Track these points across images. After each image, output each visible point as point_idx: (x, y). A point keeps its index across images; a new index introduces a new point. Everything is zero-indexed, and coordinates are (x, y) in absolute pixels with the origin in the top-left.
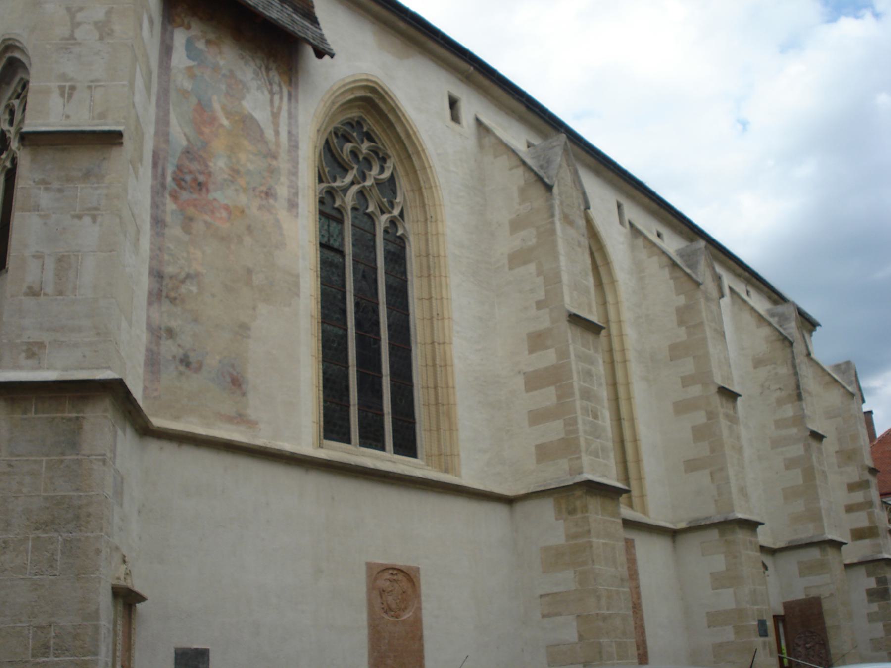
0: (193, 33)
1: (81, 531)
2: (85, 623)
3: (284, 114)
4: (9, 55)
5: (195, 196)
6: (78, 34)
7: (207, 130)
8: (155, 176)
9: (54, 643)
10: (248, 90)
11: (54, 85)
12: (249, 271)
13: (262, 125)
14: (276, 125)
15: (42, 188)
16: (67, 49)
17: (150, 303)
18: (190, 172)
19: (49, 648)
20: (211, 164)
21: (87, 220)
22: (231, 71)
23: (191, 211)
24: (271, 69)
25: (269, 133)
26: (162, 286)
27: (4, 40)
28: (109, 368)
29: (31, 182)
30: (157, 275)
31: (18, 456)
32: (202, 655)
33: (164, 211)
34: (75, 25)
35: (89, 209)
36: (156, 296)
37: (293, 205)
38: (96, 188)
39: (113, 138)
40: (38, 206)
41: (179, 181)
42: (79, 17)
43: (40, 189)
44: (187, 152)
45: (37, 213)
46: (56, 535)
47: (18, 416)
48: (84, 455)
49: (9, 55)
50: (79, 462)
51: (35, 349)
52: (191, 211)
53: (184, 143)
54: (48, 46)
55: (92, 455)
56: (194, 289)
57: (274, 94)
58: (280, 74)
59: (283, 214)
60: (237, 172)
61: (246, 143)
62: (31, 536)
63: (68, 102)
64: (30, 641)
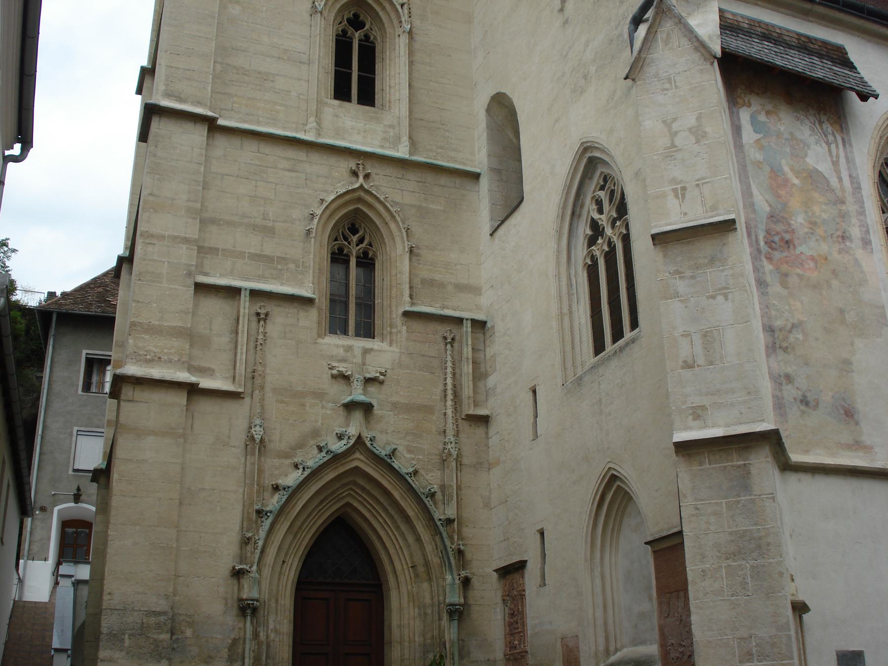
0: (755, 109)
1: (764, 558)
2: (780, 634)
3: (842, 160)
4: (588, 155)
5: (785, 254)
6: (678, 141)
7: (783, 193)
8: (751, 245)
9: (756, 651)
10: (809, 147)
11: (668, 189)
12: (842, 311)
13: (826, 175)
14: (838, 172)
16: (671, 156)
17: (768, 356)
18: (778, 233)
19: (752, 655)
20: (792, 222)
21: (720, 298)
22: (791, 133)
23: (785, 268)
24: (824, 122)
25: (834, 182)
26: (775, 339)
28: (763, 421)
29: (667, 274)
30: (769, 330)
31: (702, 500)
32: (858, 656)
33: (764, 273)
34: (673, 135)
35: (720, 290)
36: (772, 348)
37: (866, 243)
38: (722, 271)
39: (728, 226)
40: (678, 293)
41: (769, 243)
42: (675, 126)
43: (676, 278)
44: (771, 216)
46: (744, 562)
47: (696, 468)
48: (756, 495)
49: (588, 155)
50: (753, 501)
51: (699, 412)
52: (785, 268)
53: (768, 209)
54: (655, 157)
55: (762, 495)
56: (800, 337)
57: (831, 144)
58: (831, 124)
59: (860, 253)
60: (814, 223)
61: (816, 195)
62: (724, 565)
64: (736, 649)
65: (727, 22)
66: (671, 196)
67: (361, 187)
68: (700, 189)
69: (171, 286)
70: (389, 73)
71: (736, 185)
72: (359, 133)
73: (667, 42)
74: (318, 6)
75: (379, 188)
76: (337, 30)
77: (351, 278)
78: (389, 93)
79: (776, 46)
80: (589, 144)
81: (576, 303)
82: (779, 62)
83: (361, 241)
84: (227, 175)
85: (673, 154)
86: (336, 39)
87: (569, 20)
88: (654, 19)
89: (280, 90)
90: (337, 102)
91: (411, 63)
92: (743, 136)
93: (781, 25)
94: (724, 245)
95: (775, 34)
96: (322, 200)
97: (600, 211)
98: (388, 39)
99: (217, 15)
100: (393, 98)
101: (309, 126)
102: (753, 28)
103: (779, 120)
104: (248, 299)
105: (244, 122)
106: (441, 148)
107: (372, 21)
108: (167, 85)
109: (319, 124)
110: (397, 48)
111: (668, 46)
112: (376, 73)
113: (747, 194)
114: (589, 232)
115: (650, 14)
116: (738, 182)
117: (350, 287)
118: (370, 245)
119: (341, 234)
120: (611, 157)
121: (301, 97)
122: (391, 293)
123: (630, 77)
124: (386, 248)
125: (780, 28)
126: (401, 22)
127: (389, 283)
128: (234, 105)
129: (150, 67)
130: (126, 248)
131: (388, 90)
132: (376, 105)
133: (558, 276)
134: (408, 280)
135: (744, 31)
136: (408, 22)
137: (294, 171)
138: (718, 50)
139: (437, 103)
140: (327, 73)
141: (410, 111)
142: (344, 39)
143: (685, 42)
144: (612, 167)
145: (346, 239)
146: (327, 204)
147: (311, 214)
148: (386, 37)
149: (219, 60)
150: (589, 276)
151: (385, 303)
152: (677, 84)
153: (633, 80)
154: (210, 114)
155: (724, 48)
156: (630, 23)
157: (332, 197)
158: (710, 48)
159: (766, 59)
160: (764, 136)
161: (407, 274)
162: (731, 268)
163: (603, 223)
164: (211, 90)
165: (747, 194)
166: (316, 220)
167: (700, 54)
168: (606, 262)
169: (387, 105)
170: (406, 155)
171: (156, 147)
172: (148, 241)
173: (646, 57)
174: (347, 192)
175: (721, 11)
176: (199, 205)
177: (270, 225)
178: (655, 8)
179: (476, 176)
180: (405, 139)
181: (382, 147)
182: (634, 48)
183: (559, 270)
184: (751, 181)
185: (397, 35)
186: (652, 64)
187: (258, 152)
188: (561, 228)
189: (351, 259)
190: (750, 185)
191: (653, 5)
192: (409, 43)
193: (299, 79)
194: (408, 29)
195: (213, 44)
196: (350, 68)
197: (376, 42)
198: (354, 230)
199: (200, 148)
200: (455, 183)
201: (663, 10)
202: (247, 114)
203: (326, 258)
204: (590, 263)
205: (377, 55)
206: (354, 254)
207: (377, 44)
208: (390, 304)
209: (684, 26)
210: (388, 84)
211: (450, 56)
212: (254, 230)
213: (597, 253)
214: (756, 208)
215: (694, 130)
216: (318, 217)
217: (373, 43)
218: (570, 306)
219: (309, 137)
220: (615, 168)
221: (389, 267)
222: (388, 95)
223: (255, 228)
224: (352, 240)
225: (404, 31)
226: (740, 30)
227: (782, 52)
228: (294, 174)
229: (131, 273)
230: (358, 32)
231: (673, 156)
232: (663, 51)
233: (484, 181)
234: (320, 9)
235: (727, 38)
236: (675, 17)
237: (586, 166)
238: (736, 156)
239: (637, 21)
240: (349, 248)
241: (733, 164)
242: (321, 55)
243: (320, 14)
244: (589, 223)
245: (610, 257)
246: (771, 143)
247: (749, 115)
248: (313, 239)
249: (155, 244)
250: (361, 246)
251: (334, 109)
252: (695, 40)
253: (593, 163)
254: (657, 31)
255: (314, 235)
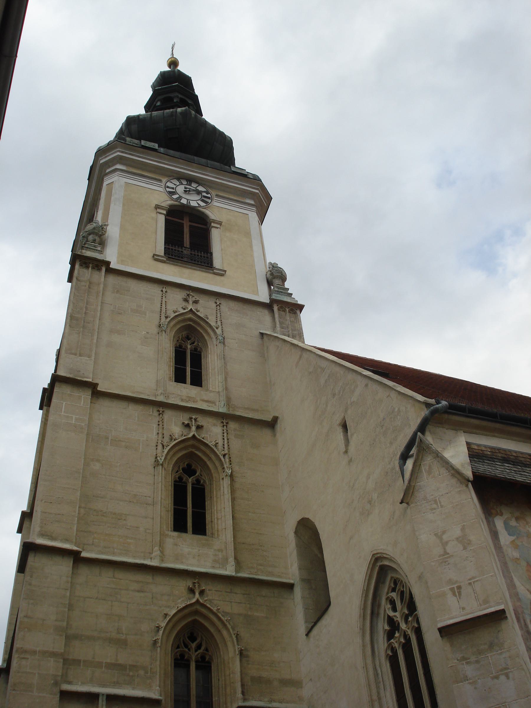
0: (506, 517)
4: (379, 564)
6: (449, 549)
8: (521, 628)
11: (446, 589)
15: (465, 663)
21: (503, 678)
27: (373, 555)
29: (456, 661)
34: (445, 544)
35: (501, 670)
38: (501, 653)
42: (445, 537)
43: (463, 664)
45: (467, 682)
49: (379, 564)
54: (433, 564)
63: (460, 598)
65: (474, 452)
66: (450, 595)
67: (198, 601)
68: (472, 587)
69: (41, 694)
70: (217, 509)
71: (502, 581)
72: (194, 558)
73: (429, 472)
74: (159, 460)
75: (213, 601)
76: (175, 477)
77: (191, 680)
78: (217, 524)
79: (514, 466)
80: (379, 555)
81: (383, 690)
82: (519, 478)
83: (199, 647)
84: (88, 598)
85: (446, 560)
86: (174, 484)
87: (353, 459)
88: (418, 455)
89: (131, 526)
90: (176, 534)
91: (233, 499)
92: (500, 539)
93: (516, 450)
94: (499, 632)
95: (512, 457)
96: (166, 615)
97: (394, 609)
98: (214, 482)
99: (82, 471)
100: (220, 528)
101: (154, 554)
102: (495, 454)
103: (527, 524)
104: (104, 703)
105: (102, 553)
106: (261, 565)
107: (202, 469)
108: (41, 527)
109: (162, 552)
110: (222, 488)
111: (431, 476)
112: (206, 508)
113: (511, 586)
114: (387, 627)
115: (414, 451)
116: (503, 577)
117: (191, 688)
118: (207, 650)
119: (182, 642)
120: (399, 565)
121: (148, 531)
122: (225, 691)
123: (404, 501)
124: (220, 652)
125: (516, 452)
126: (224, 468)
127: (223, 683)
128: (94, 540)
129: (29, 511)
130: (4, 661)
131: (216, 521)
132: (207, 534)
133: (366, 667)
134: (239, 679)
135: (488, 458)
136: (229, 468)
137: (143, 592)
138: (469, 474)
139: (255, 529)
140: (168, 511)
141: (235, 537)
142: (180, 484)
143: (443, 471)
144: (399, 572)
145: (186, 646)
146: (170, 617)
147: (157, 627)
148: (213, 481)
149: (83, 505)
150: (391, 666)
151: (221, 700)
152: (442, 504)
153: (408, 503)
154: (75, 548)
155: (475, 472)
156: (400, 459)
157: (174, 611)
158: (464, 474)
159: (509, 477)
160: (517, 537)
161: (239, 674)
162: (508, 651)
163: (397, 619)
164: (77, 528)
165: (511, 586)
166: (161, 632)
167: (456, 479)
168: (404, 652)
169: (216, 533)
170: (233, 573)
171: (31, 577)
172: (22, 656)
173: (415, 485)
174: (184, 608)
175: (468, 444)
176: (65, 624)
177: (123, 638)
178: (417, 447)
179: (290, 587)
180: (231, 560)
181: (213, 567)
182: (405, 478)
183: (365, 662)
184: (513, 574)
185: (221, 478)
186: (420, 490)
187: (114, 577)
188: (364, 625)
189: (191, 663)
190: (512, 579)
191: (415, 444)
192: (231, 484)
193: (146, 518)
194: (230, 474)
195: (79, 494)
196: (186, 506)
197: (205, 485)
198: (193, 638)
199: (67, 577)
200: (274, 593)
201: (424, 448)
202: (105, 547)
203: (170, 663)
204: (391, 654)
205: (206, 494)
206: (194, 658)
207: (206, 486)
208: (226, 701)
209: (441, 459)
210: (216, 516)
211: (263, 491)
212: (110, 643)
213: (396, 645)
214: (520, 597)
215: (461, 539)
216: (163, 629)
217: (203, 485)
218: (379, 693)
219: (154, 563)
220: (402, 573)
221: (223, 668)
222: (216, 526)
223: (111, 641)
224: (191, 647)
225: (227, 475)
226: (485, 457)
227: (520, 470)
228: (142, 594)
229: (7, 683)
230: (191, 478)
231: (447, 561)
232: (427, 480)
233: (298, 591)
234: (161, 463)
235: (475, 465)
236: (433, 453)
237: (378, 573)
238: (498, 556)
239: (404, 457)
240: (189, 654)
241: (496, 563)
242: (163, 497)
243: (161, 466)
244: (386, 621)
245: (407, 647)
246: (524, 543)
247: (503, 522)
248: (159, 649)
249: (28, 659)
250: (199, 651)
251: (174, 539)
252: (451, 469)
253: (384, 571)
254: (420, 465)
255: (159, 644)
